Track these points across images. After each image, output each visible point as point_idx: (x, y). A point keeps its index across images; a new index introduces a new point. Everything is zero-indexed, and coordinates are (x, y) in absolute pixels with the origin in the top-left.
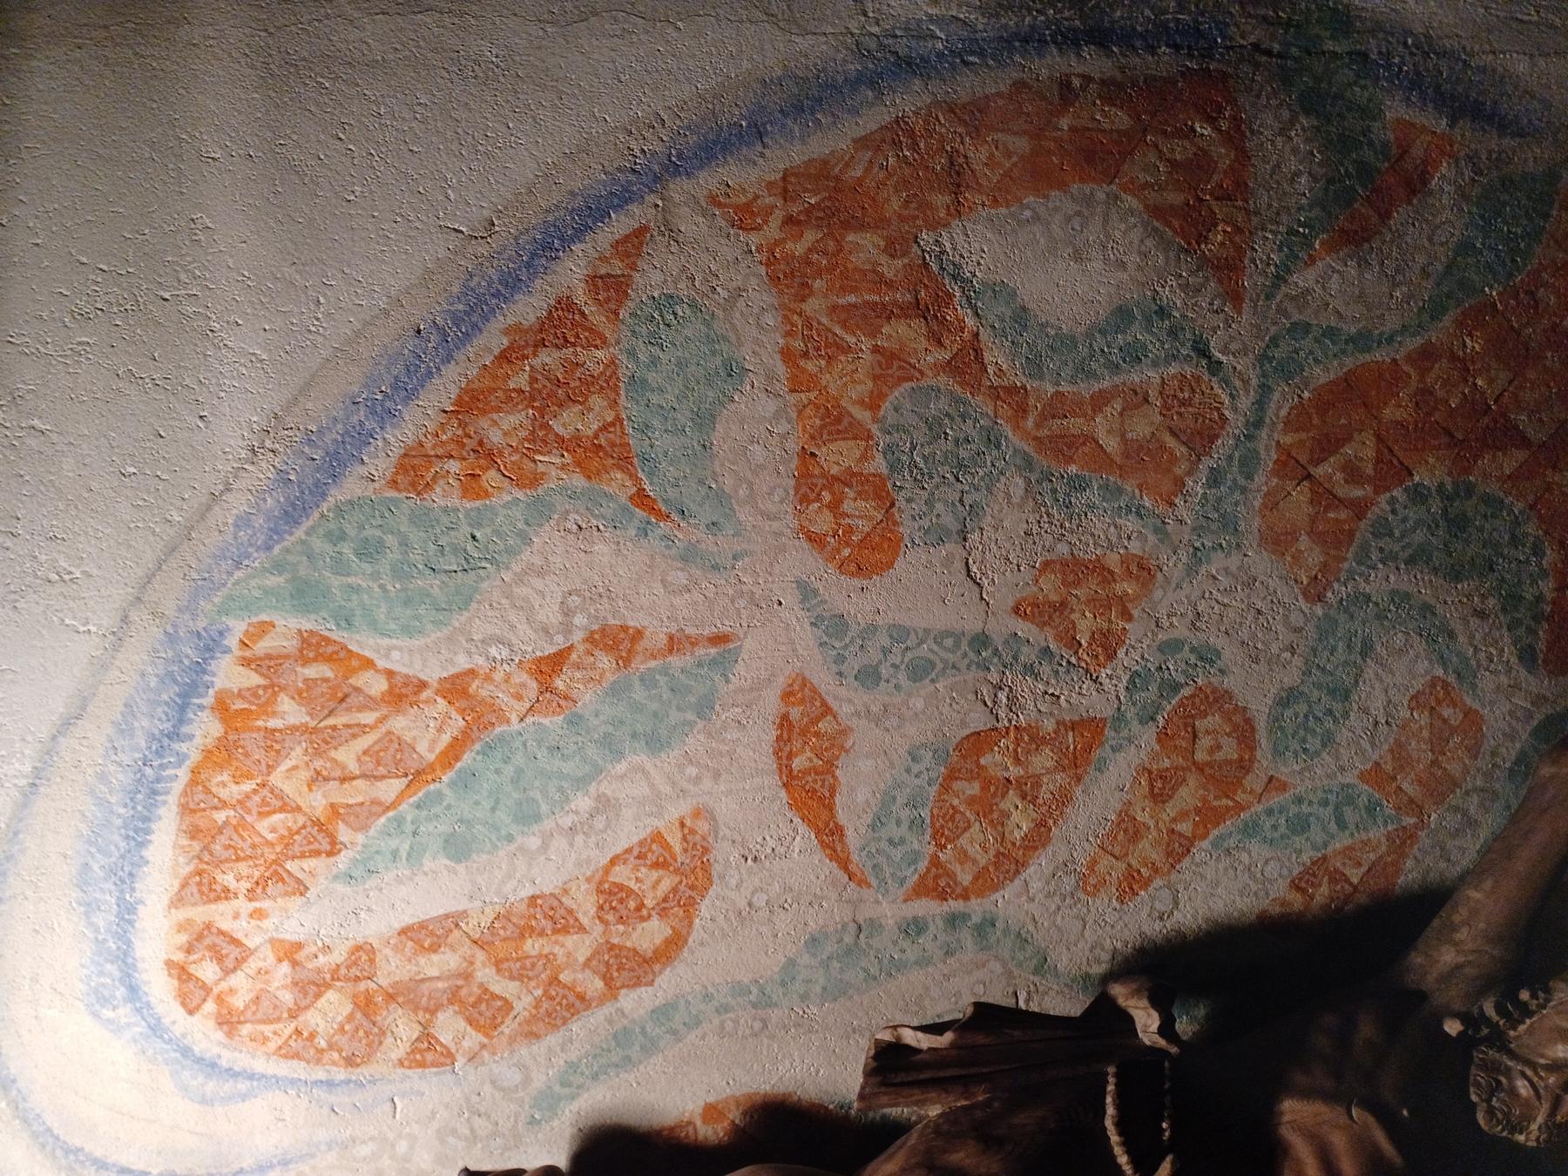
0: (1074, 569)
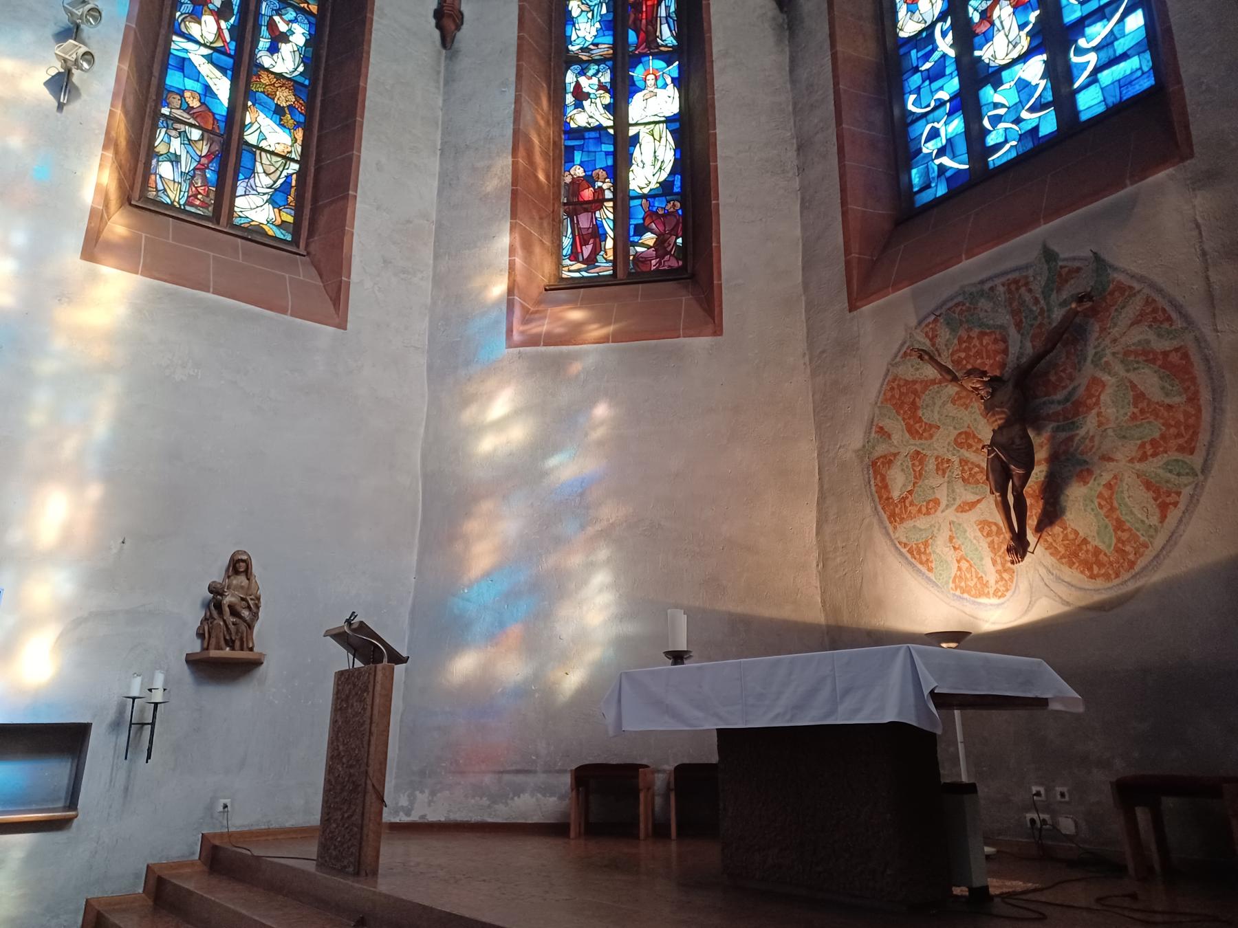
0: (938, 469)
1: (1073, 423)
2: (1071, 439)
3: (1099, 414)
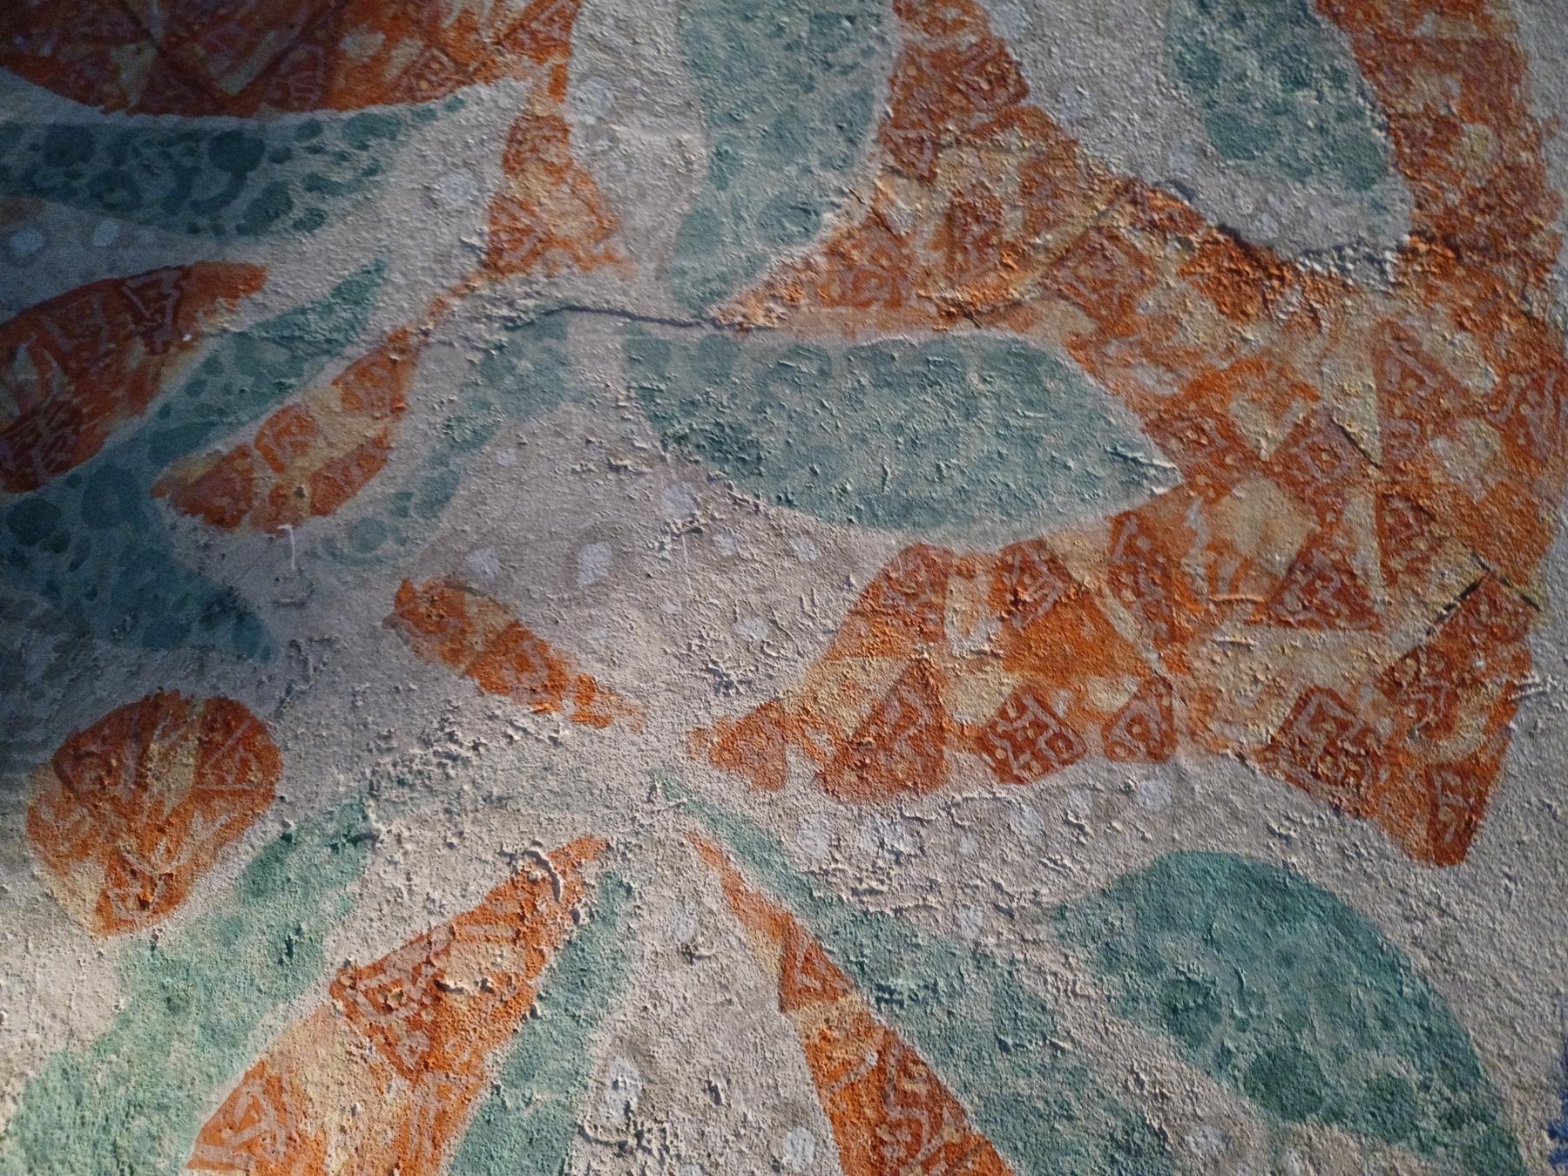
1: (240, 156)
2: (155, 307)
3: (525, 143)
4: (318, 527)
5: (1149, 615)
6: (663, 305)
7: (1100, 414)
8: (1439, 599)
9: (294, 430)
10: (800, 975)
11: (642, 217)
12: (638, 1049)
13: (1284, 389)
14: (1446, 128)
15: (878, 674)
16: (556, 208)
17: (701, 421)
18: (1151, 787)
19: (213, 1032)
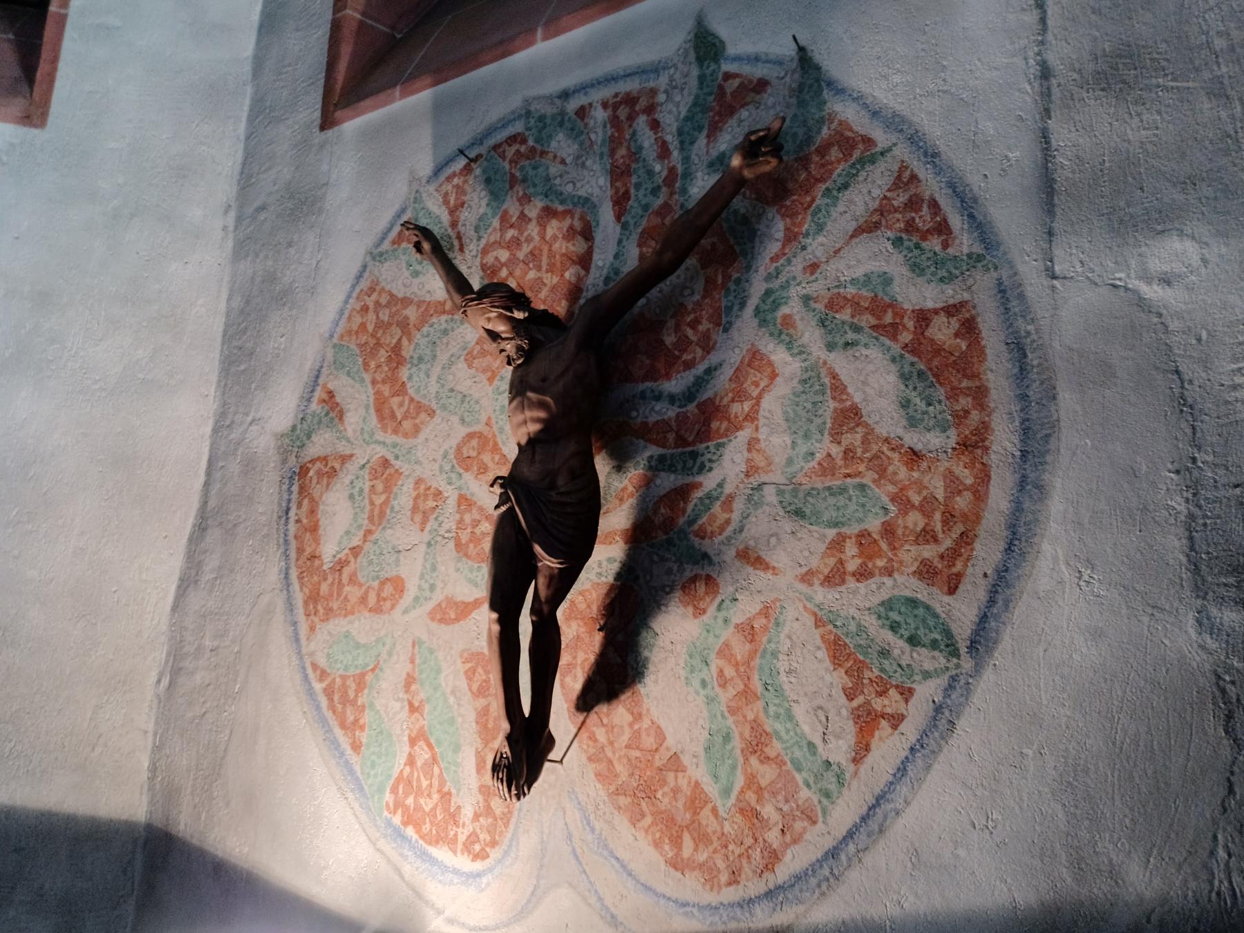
2: (683, 493)
3: (752, 444)
4: (720, 538)
5: (889, 544)
6: (783, 481)
7: (879, 498)
8: (954, 536)
9: (713, 518)
10: (819, 623)
11: (777, 460)
12: (789, 637)
13: (920, 487)
14: (967, 412)
15: (832, 561)
16: (759, 460)
17: (793, 507)
18: (888, 582)
19: (716, 636)
